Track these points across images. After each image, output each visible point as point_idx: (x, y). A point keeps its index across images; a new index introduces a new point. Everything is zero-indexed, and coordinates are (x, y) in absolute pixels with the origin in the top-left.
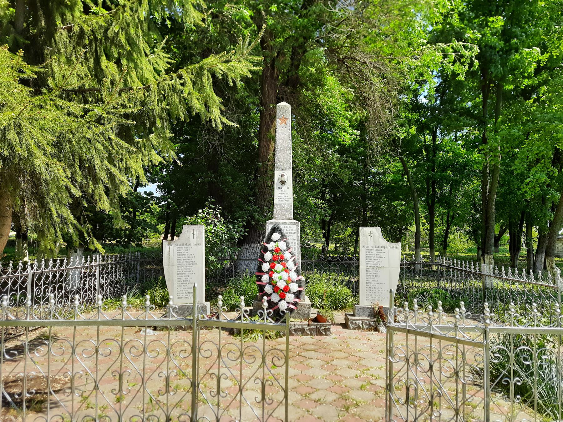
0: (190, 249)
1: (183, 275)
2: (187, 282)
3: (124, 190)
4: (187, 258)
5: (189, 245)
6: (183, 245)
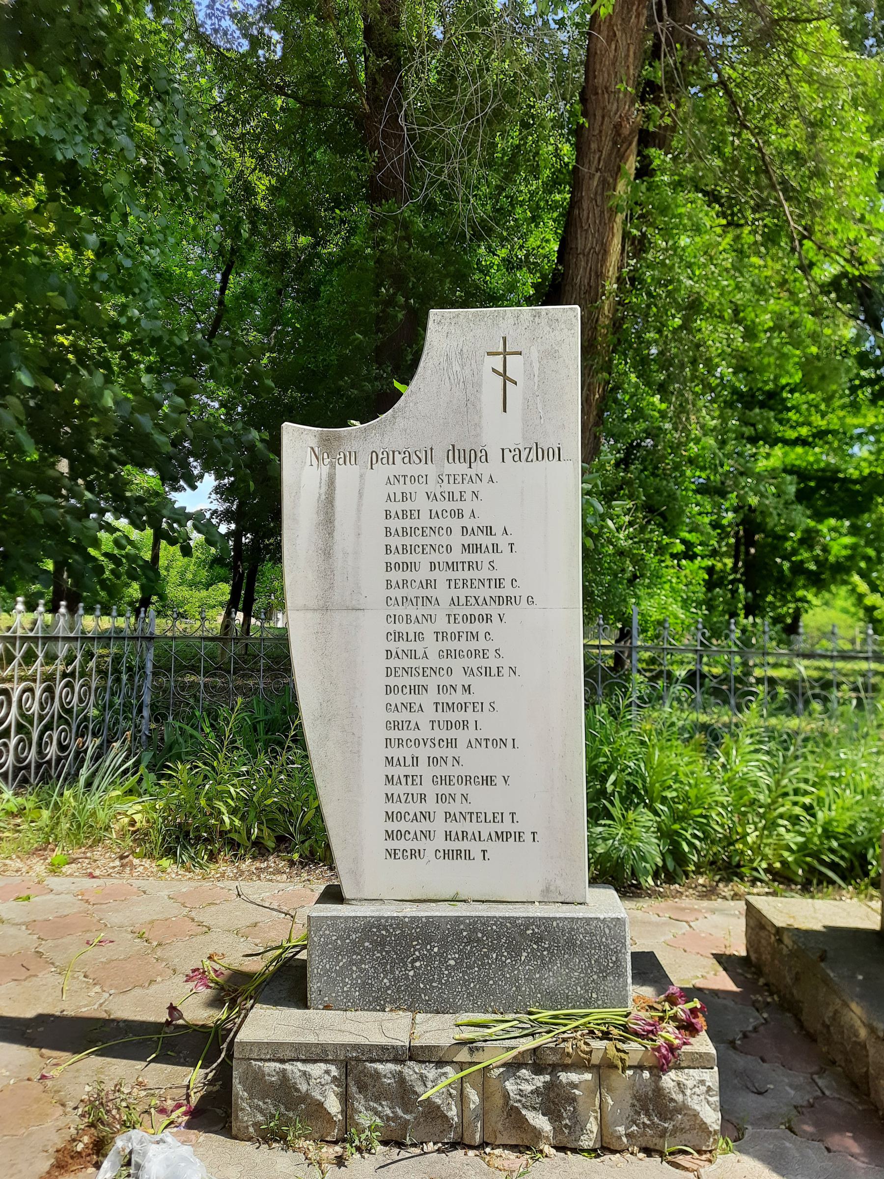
0: (481, 487)
1: (432, 682)
2: (463, 737)
3: (87, 280)
4: (457, 555)
5: (472, 456)
6: (428, 456)
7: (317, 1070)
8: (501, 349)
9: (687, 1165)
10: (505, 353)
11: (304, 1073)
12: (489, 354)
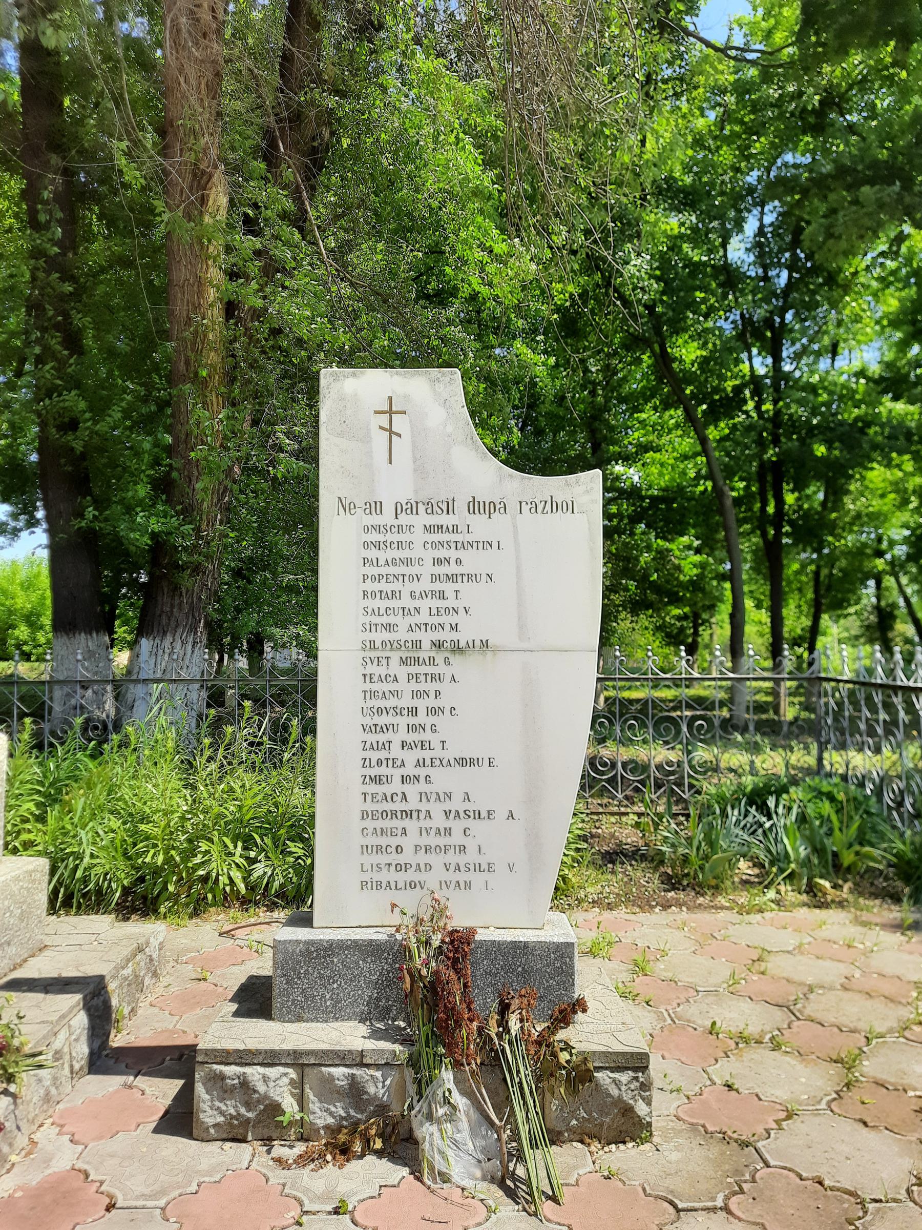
7: (273, 1072)
8: (387, 408)
9: (543, 1174)
10: (391, 412)
11: (264, 1076)
12: (376, 412)
